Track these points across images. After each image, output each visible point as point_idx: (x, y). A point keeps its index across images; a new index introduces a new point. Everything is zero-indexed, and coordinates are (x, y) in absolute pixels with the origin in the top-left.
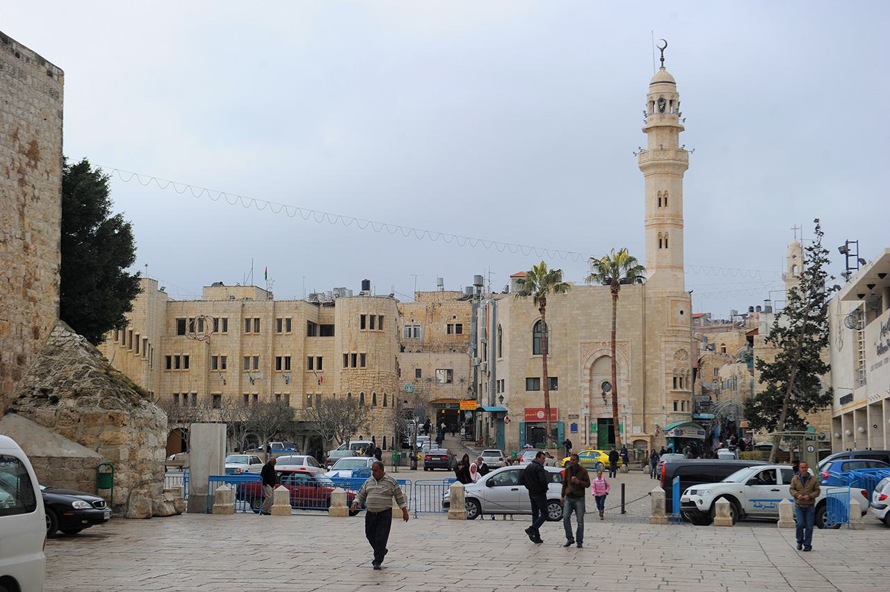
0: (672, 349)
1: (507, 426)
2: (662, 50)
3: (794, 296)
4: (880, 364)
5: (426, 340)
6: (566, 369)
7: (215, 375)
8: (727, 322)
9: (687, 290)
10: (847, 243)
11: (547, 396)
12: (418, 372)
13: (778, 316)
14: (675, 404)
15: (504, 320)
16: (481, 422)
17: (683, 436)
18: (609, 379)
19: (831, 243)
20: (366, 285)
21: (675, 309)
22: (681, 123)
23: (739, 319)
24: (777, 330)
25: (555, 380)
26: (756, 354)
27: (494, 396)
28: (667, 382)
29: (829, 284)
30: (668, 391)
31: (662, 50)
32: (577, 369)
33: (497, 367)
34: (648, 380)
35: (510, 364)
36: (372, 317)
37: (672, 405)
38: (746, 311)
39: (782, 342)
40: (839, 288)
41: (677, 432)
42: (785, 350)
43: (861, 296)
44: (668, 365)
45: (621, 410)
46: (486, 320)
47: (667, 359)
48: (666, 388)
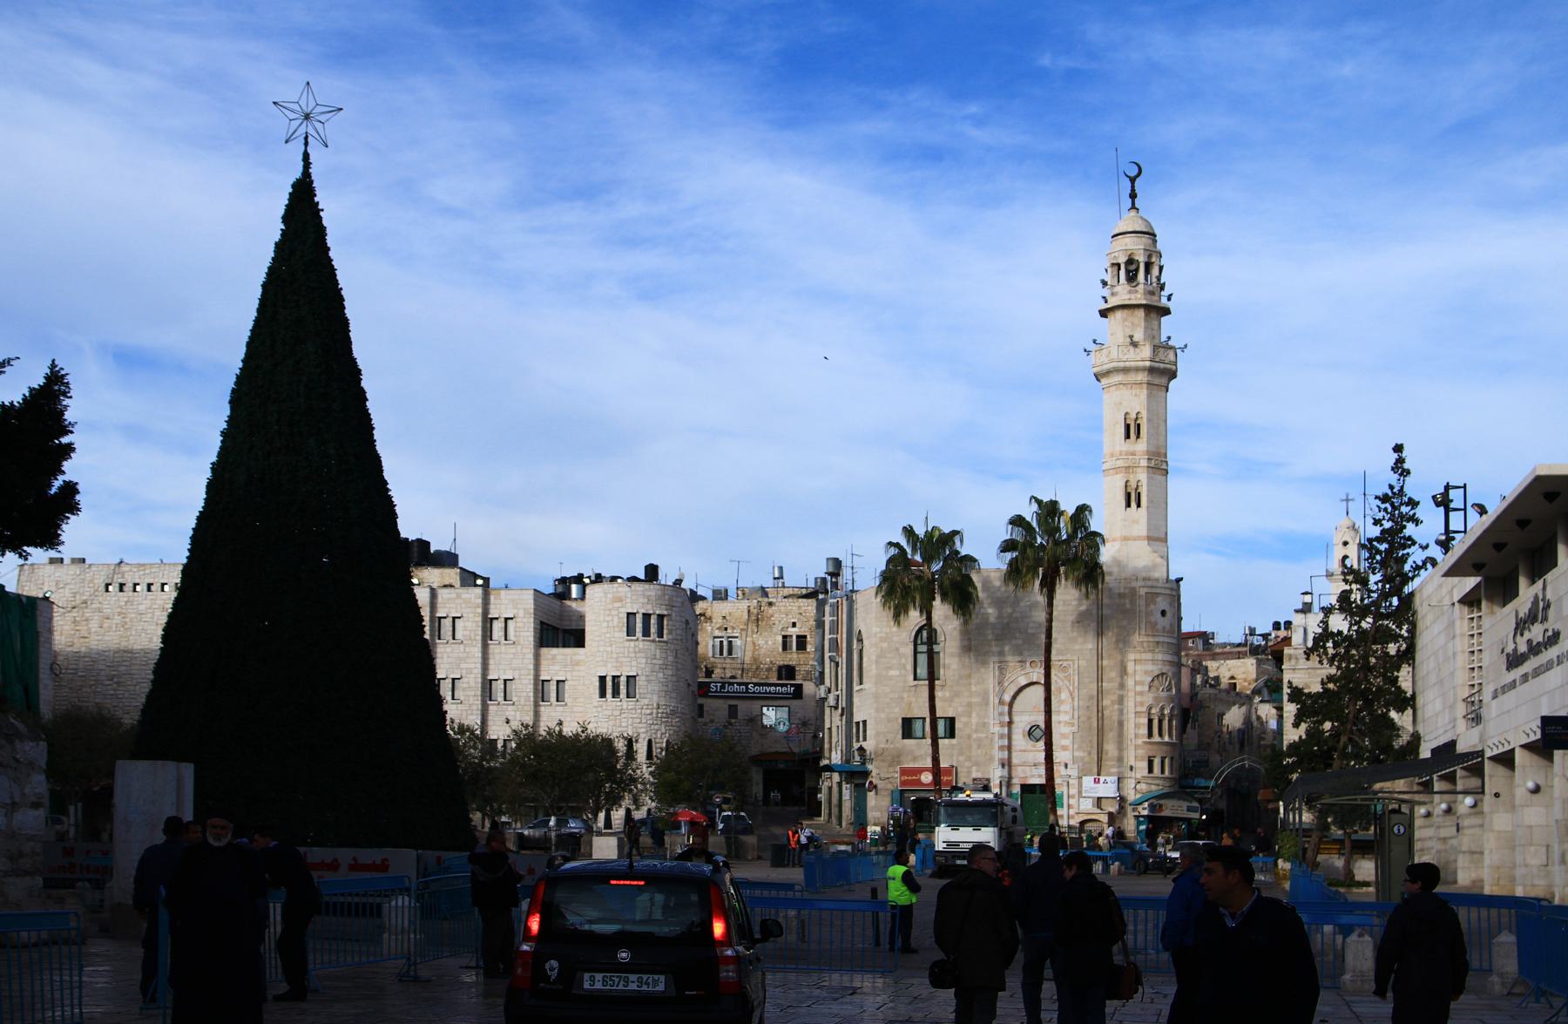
0: (1146, 672)
1: (871, 795)
2: (1133, 180)
3: (1354, 576)
4: (1513, 685)
5: (747, 660)
6: (970, 705)
8: (1239, 645)
9: (1173, 577)
10: (1447, 487)
13: (1327, 611)
14: (1151, 763)
16: (830, 788)
17: (1163, 814)
18: (1040, 720)
21: (1152, 607)
22: (1164, 300)
23: (1258, 641)
24: (1325, 635)
25: (951, 722)
26: (1286, 677)
28: (1137, 726)
29: (1416, 555)
30: (1140, 742)
31: (1133, 180)
32: (987, 704)
33: (856, 700)
36: (646, 617)
37: (1145, 764)
38: (1268, 628)
39: (1334, 656)
40: (1434, 562)
41: (1152, 807)
42: (1338, 668)
44: (1139, 698)
45: (1059, 771)
47: (1138, 688)
48: (1136, 736)
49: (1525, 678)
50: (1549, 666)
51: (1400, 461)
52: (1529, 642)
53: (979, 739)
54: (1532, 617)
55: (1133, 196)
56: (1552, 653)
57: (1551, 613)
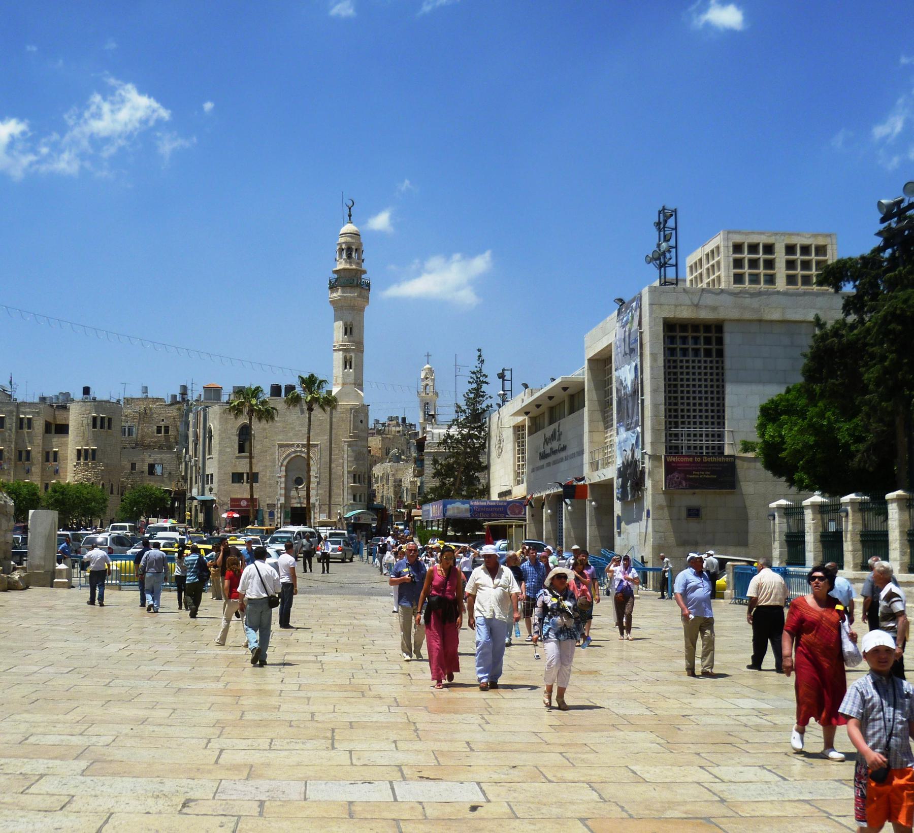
4: (542, 467)
7: (49, 465)
10: (504, 370)
11: (251, 488)
12: (133, 466)
15: (214, 424)
19: (491, 371)
20: (86, 391)
27: (203, 487)
34: (333, 476)
35: (219, 461)
43: (527, 413)
46: (196, 425)
49: (549, 465)
50: (561, 460)
51: (480, 356)
52: (551, 449)
53: (270, 484)
54: (553, 437)
55: (350, 216)
56: (563, 455)
57: (562, 437)
